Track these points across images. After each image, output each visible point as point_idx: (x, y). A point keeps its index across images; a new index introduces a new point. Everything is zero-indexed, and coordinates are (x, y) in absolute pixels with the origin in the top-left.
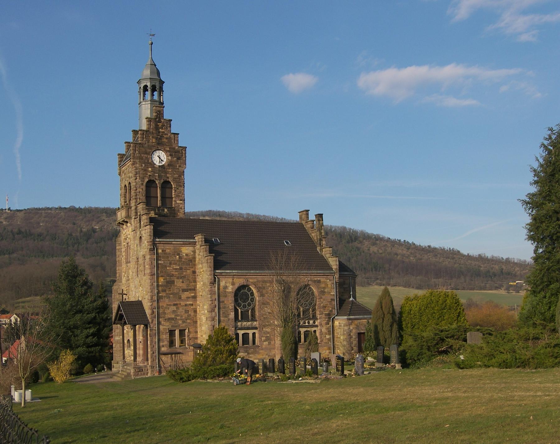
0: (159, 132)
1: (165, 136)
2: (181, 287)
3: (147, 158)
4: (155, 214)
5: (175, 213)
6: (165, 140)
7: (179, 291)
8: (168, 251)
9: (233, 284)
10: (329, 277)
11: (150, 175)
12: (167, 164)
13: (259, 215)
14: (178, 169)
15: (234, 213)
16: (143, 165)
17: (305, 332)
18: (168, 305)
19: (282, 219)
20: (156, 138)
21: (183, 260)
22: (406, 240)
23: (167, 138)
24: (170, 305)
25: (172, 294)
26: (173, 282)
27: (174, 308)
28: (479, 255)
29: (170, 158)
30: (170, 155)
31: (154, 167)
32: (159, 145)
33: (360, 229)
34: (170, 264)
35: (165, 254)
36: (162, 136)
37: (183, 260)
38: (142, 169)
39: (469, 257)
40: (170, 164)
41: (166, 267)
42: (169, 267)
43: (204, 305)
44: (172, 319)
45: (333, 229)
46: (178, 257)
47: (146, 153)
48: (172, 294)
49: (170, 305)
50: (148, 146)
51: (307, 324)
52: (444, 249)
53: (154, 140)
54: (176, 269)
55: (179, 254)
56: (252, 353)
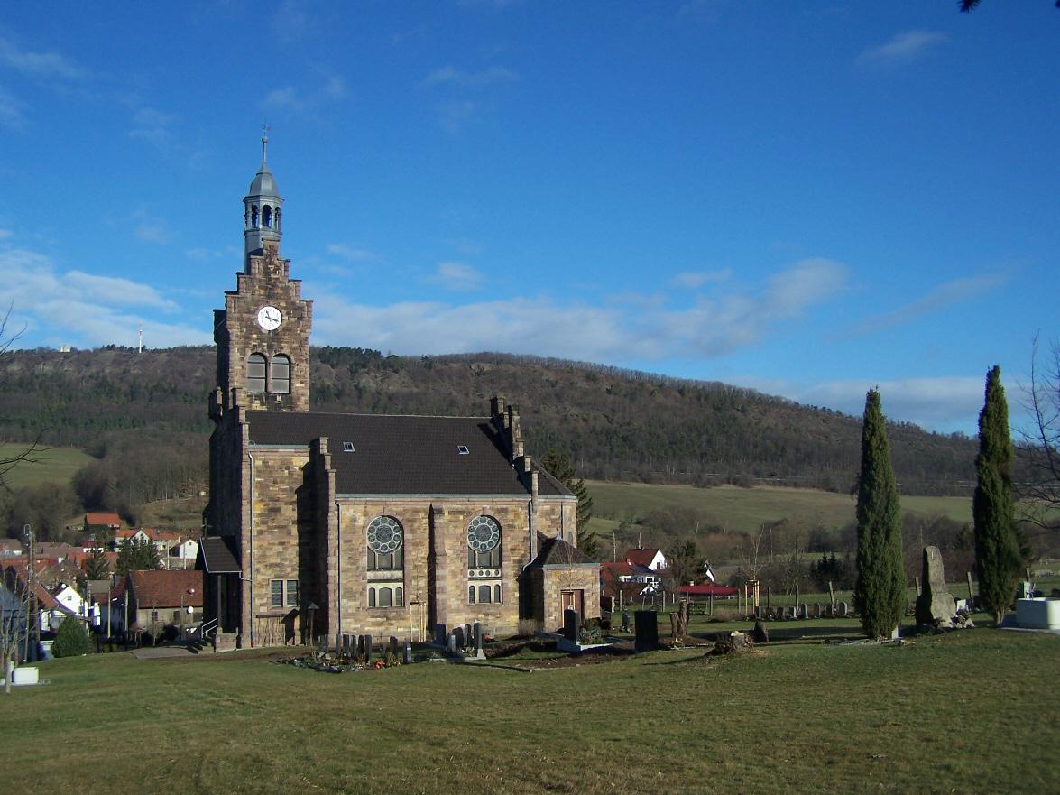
0: (270, 279)
1: (280, 285)
2: (290, 518)
3: (249, 319)
4: (262, 404)
5: (292, 403)
6: (279, 291)
7: (289, 523)
8: (271, 463)
9: (366, 514)
10: (521, 503)
11: (254, 346)
12: (281, 328)
13: (571, 362)
14: (299, 335)
15: (527, 356)
16: (245, 330)
17: (380, 590)
18: (269, 544)
19: (611, 367)
20: (266, 289)
21: (295, 476)
22: (827, 407)
23: (281, 288)
24: (274, 544)
25: (276, 527)
26: (279, 510)
27: (280, 548)
28: (954, 434)
29: (286, 318)
30: (288, 314)
31: (261, 333)
32: (270, 297)
33: (747, 387)
34: (275, 482)
35: (267, 467)
36: (274, 286)
37: (295, 476)
38: (243, 336)
39: (935, 438)
40: (286, 329)
41: (268, 486)
42: (274, 486)
43: (72, 577)
44: (277, 565)
45: (700, 387)
46: (286, 471)
47: (249, 312)
48: (276, 527)
49: (274, 544)
50: (253, 300)
51: (484, 575)
52: (892, 423)
53: (262, 292)
54: (283, 490)
55: (288, 468)
56: (394, 618)
